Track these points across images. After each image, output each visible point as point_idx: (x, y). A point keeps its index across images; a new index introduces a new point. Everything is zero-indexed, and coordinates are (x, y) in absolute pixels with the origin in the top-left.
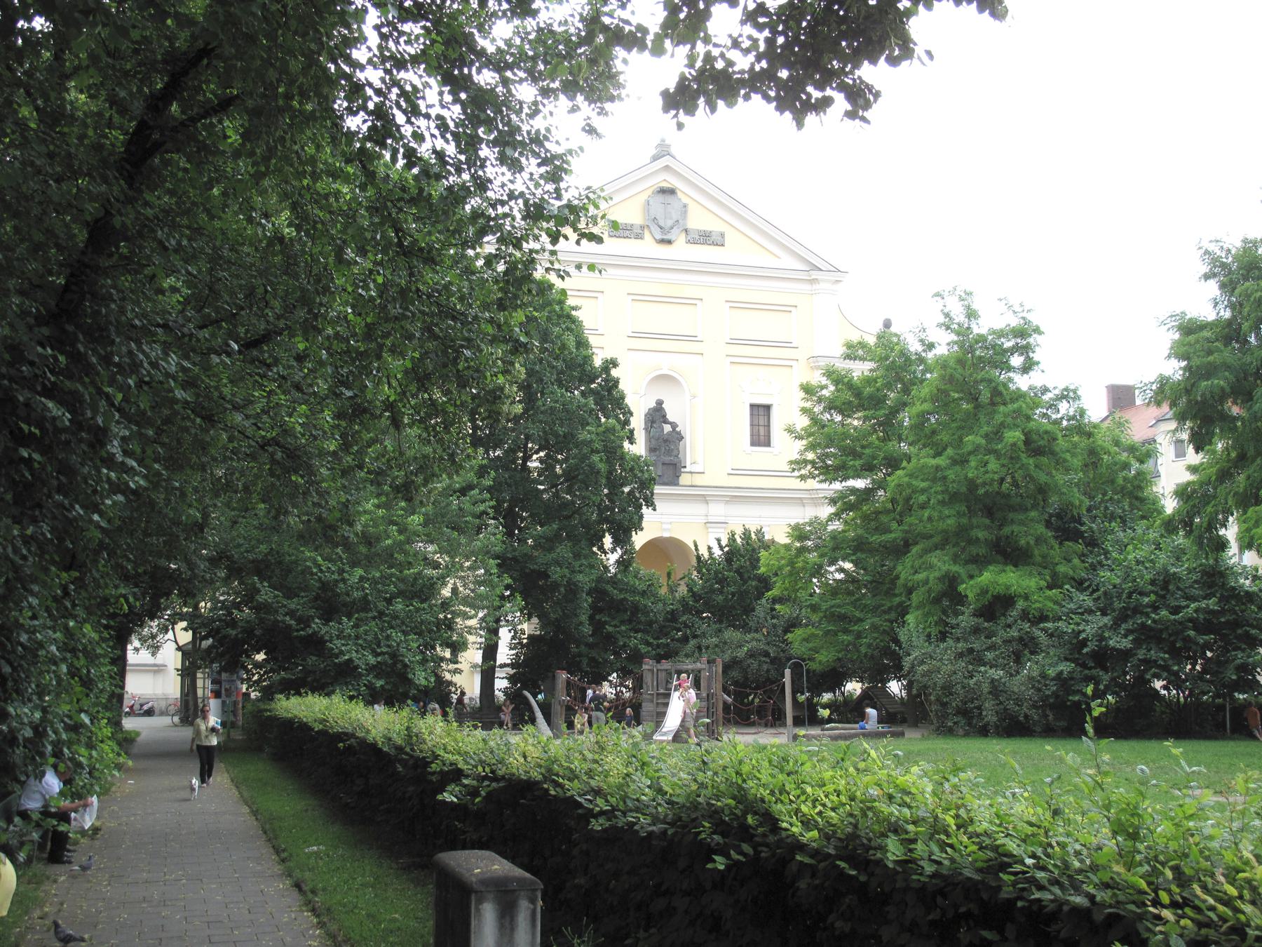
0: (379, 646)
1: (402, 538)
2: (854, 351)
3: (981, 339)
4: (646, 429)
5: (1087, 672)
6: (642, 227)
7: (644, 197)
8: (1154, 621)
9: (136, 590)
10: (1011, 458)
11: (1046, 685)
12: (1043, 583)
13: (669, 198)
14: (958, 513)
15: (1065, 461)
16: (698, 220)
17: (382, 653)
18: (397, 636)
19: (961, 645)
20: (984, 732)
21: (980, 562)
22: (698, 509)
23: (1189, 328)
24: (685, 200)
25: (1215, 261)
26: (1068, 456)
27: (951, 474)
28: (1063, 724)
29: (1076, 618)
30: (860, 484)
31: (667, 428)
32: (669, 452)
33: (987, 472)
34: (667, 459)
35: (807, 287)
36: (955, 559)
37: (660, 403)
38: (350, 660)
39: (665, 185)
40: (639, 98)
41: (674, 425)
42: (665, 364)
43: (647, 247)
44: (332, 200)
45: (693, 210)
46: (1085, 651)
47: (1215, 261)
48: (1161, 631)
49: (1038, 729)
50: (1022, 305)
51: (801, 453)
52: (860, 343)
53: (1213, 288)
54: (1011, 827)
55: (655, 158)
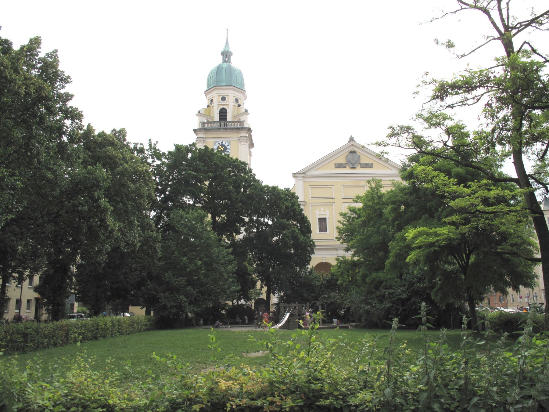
2: (358, 199)
6: (346, 164)
7: (346, 154)
13: (354, 154)
16: (364, 160)
24: (359, 154)
38: (165, 305)
39: (352, 150)
44: (211, 376)
55: (349, 142)
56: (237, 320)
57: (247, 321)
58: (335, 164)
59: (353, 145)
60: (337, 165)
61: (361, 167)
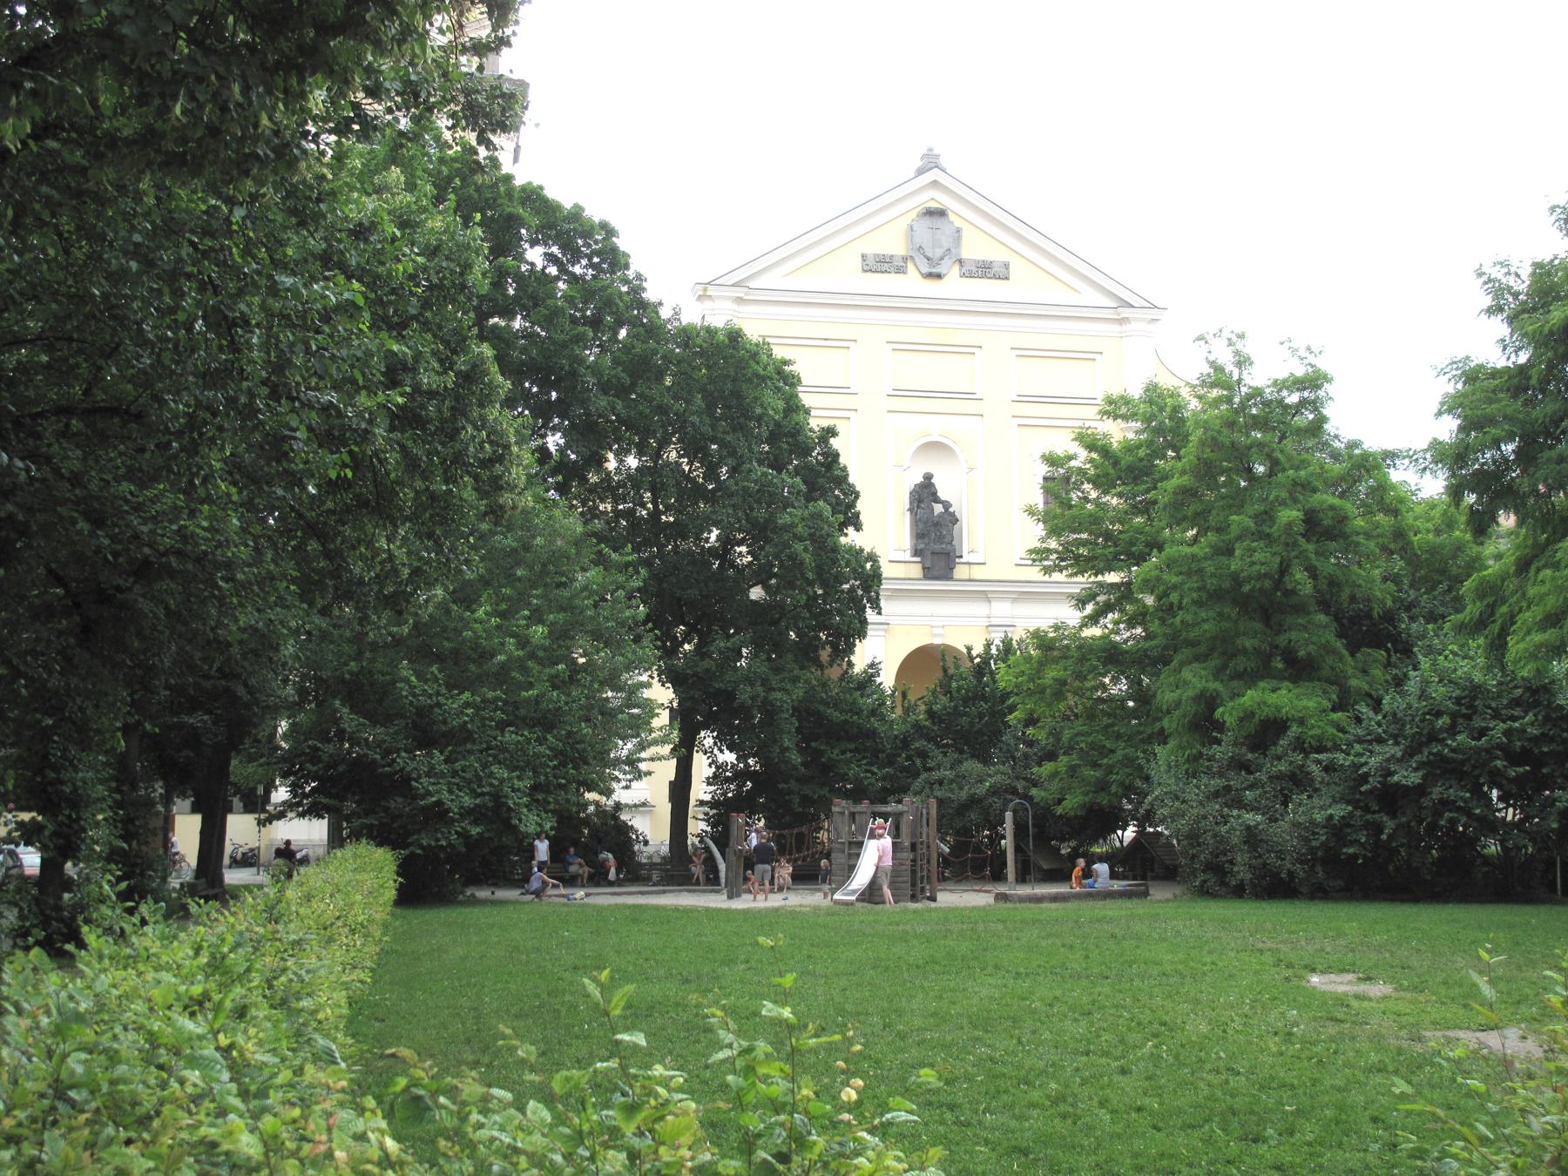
0: (480, 786)
1: (521, 653)
2: (1115, 408)
3: (1257, 393)
4: (911, 510)
5: (1369, 817)
6: (905, 259)
7: (908, 219)
8: (1453, 750)
9: (206, 717)
10: (1287, 544)
11: (1314, 833)
12: (1327, 704)
13: (938, 222)
14: (1220, 615)
15: (1358, 544)
16: (975, 247)
17: (483, 794)
18: (501, 772)
19: (1217, 783)
20: (1239, 892)
21: (1249, 678)
22: (978, 609)
23: (1472, 375)
24: (958, 223)
25: (1499, 291)
26: (1361, 539)
27: (1209, 567)
28: (1340, 883)
29: (1358, 747)
30: (1113, 578)
31: (938, 508)
32: (941, 538)
33: (1254, 563)
34: (937, 547)
35: (1115, 328)
36: (1217, 674)
37: (928, 477)
38: (439, 803)
40: (537, 125)
41: (947, 505)
42: (935, 429)
43: (911, 283)
45: (968, 235)
46: (1363, 789)
47: (1499, 291)
48: (1463, 762)
49: (1304, 890)
50: (1309, 348)
51: (1043, 540)
52: (1122, 397)
53: (1499, 328)
54: (129, 1044)
55: (920, 172)
56: (573, 869)
57: (612, 875)
58: (864, 257)
59: (935, 184)
60: (871, 261)
61: (963, 275)
